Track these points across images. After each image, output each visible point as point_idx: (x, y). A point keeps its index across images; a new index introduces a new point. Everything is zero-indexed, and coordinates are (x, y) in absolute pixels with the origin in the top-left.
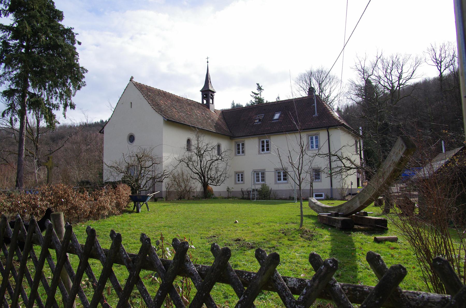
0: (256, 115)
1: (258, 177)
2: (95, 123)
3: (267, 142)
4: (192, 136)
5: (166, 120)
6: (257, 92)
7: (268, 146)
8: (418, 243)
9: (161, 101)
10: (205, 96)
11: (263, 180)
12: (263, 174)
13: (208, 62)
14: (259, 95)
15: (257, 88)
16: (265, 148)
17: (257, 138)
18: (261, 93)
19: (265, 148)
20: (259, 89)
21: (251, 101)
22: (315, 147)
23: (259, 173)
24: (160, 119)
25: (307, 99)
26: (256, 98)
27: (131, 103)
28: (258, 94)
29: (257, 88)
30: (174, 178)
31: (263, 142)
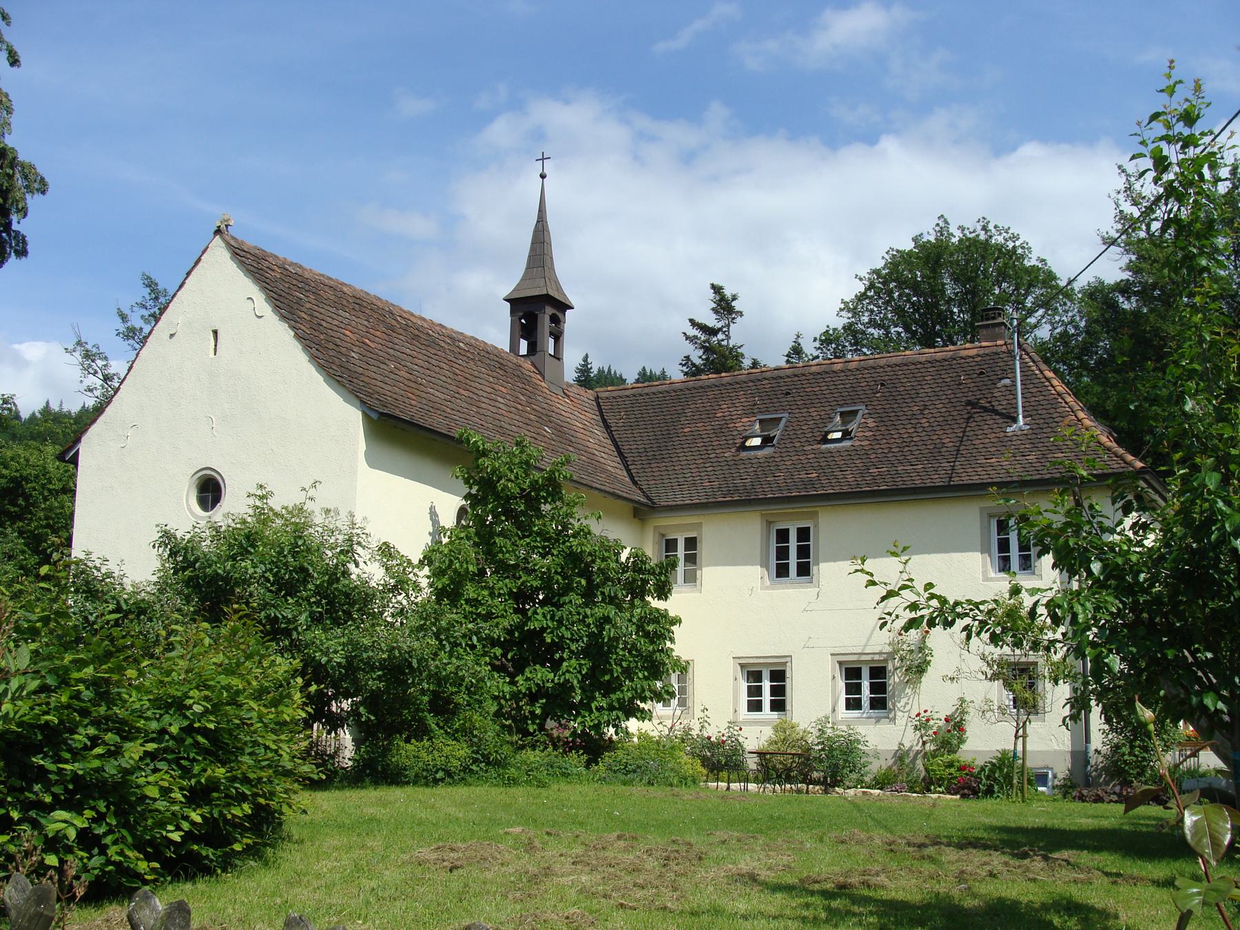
0: (747, 415)
1: (755, 691)
2: (645, 377)
3: (804, 534)
4: (996, 503)
5: (374, 416)
6: (711, 321)
7: (804, 552)
8: (267, 762)
9: (348, 333)
10: (523, 321)
11: (778, 706)
12: (779, 676)
13: (543, 176)
14: (720, 336)
15: (714, 305)
16: (793, 561)
17: (758, 513)
18: (728, 326)
19: (793, 561)
20: (724, 309)
21: (687, 358)
22: (681, 545)
23: (760, 673)
24: (352, 418)
25: (978, 355)
26: (708, 349)
27: (215, 332)
28: (720, 330)
29: (714, 305)
30: (831, 749)
31: (783, 535)
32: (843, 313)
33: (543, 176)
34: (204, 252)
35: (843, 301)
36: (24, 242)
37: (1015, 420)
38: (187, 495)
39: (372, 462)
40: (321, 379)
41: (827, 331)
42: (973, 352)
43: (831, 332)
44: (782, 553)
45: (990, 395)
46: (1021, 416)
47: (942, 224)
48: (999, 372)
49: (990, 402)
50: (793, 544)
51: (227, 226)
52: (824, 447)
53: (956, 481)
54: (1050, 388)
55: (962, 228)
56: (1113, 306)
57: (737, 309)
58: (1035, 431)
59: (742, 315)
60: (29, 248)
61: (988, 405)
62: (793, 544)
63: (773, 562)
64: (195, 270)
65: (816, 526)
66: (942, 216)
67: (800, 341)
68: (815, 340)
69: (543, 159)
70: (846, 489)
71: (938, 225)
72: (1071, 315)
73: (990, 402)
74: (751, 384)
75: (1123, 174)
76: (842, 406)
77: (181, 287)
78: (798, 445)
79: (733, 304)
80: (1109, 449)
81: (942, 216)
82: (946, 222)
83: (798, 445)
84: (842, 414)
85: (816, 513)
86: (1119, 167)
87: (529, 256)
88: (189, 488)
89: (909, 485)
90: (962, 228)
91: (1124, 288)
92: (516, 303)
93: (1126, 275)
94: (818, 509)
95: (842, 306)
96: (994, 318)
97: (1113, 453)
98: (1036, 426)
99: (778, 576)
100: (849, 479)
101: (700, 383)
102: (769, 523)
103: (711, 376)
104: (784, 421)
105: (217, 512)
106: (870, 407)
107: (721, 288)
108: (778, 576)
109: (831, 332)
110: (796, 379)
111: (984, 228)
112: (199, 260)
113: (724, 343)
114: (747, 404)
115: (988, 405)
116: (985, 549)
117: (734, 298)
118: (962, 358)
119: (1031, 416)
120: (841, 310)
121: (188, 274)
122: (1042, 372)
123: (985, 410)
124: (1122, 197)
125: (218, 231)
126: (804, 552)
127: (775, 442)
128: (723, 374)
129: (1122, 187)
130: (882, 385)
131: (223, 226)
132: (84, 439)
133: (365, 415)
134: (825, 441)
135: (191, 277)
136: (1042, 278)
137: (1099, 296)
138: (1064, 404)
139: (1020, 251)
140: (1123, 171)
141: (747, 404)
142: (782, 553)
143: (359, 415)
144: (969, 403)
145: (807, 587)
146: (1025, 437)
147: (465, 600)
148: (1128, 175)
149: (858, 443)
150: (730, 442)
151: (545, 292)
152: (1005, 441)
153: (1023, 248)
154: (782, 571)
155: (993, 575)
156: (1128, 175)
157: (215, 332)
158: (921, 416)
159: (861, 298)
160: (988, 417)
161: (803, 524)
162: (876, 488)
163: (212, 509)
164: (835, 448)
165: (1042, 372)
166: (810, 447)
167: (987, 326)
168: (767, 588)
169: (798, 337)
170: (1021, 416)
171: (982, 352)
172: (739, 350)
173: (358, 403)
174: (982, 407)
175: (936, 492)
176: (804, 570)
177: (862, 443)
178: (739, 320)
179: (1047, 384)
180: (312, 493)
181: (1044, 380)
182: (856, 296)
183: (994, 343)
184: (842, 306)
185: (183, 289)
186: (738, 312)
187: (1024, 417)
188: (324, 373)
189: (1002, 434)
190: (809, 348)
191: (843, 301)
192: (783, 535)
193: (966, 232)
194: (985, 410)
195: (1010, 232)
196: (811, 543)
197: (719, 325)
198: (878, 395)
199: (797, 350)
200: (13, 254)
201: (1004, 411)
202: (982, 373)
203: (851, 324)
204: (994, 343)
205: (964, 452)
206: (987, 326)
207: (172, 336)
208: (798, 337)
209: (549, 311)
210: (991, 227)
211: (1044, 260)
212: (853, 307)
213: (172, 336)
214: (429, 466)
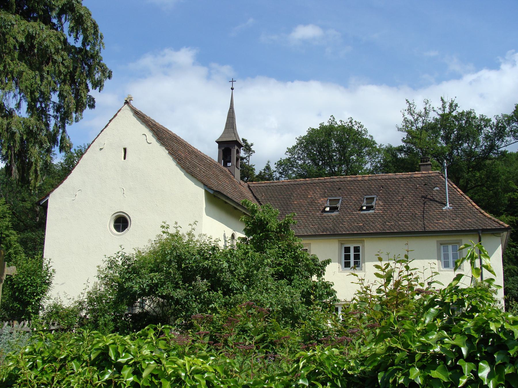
3: (357, 249)
7: (357, 257)
13: (232, 89)
17: (337, 240)
20: (247, 149)
24: (200, 192)
27: (125, 150)
28: (245, 158)
31: (347, 250)
32: (288, 153)
33: (232, 89)
34: (119, 111)
35: (288, 148)
36: (94, 102)
37: (445, 205)
38: (110, 224)
39: (208, 214)
40: (183, 174)
41: (281, 160)
42: (419, 175)
43: (282, 161)
44: (347, 257)
45: (431, 194)
46: (448, 203)
47: (332, 119)
48: (433, 184)
49: (432, 197)
50: (352, 254)
51: (130, 100)
52: (362, 212)
53: (427, 229)
54: (457, 192)
55: (341, 121)
56: (395, 156)
57: (253, 149)
58: (455, 210)
59: (254, 152)
60: (96, 104)
61: (431, 198)
62: (352, 254)
63: (343, 261)
64: (114, 119)
65: (363, 246)
66: (332, 116)
67: (269, 164)
68: (275, 164)
69: (232, 81)
70: (378, 231)
71: (330, 119)
72: (380, 158)
73: (432, 197)
74: (321, 184)
75: (408, 103)
76: (366, 195)
77: (106, 127)
78: (350, 211)
79: (251, 147)
80: (490, 218)
81: (332, 116)
82: (334, 118)
83: (350, 211)
84: (367, 199)
85: (364, 241)
86: (407, 100)
87: (226, 123)
88: (111, 220)
89: (407, 230)
90: (341, 121)
91: (400, 149)
92: (220, 143)
93: (403, 144)
94: (364, 239)
95: (287, 150)
96: (426, 162)
97: (493, 220)
98: (455, 208)
99: (345, 267)
100: (378, 227)
101: (297, 183)
102: (342, 244)
103: (301, 179)
104: (341, 200)
105: (125, 233)
106: (379, 196)
107: (246, 140)
108: (345, 267)
109: (282, 161)
110: (342, 183)
111: (351, 122)
112: (116, 115)
113: (247, 164)
114: (321, 192)
115: (431, 198)
116: (439, 258)
117: (252, 145)
118: (415, 178)
119: (452, 203)
120: (287, 152)
121: (110, 121)
122: (452, 185)
123: (431, 200)
124: (406, 113)
125: (127, 102)
126: (357, 257)
127: (339, 209)
128: (307, 179)
129: (407, 108)
130: (382, 187)
131: (128, 100)
132: (51, 195)
133: (206, 192)
134: (361, 209)
135: (111, 122)
136: (370, 144)
137: (390, 151)
138: (465, 199)
139: (363, 132)
140: (408, 102)
141: (321, 192)
142: (347, 257)
143: (203, 191)
144: (423, 197)
145: (360, 272)
146: (451, 212)
147: (162, 271)
148: (410, 104)
149: (377, 212)
150: (318, 208)
151: (235, 140)
152: (444, 214)
153: (365, 131)
154: (347, 265)
155: (442, 269)
156: (410, 104)
157: (125, 150)
158: (403, 201)
159: (294, 147)
160: (433, 203)
161: (356, 245)
162: (392, 231)
163: (123, 231)
164: (367, 213)
165: (452, 185)
166: (356, 212)
167: (424, 165)
168: (341, 272)
169: (269, 162)
170: (448, 203)
171: (423, 175)
172: (253, 167)
173: (202, 185)
174: (429, 199)
175: (402, 234)
176: (357, 264)
177: (379, 212)
178: (253, 154)
179: (455, 190)
180: (194, 226)
181: (453, 188)
182: (293, 146)
183: (428, 172)
184: (287, 150)
185: (107, 128)
186: (253, 151)
187: (449, 204)
188: (184, 171)
189: (441, 210)
190: (273, 167)
191: (288, 148)
192: (347, 250)
193: (343, 123)
194: (431, 200)
195: (361, 124)
196: (360, 253)
197: (245, 156)
198: (381, 191)
199: (268, 168)
200: (87, 107)
201: (439, 201)
202: (425, 184)
203: (290, 158)
204: (428, 172)
205: (427, 217)
206: (424, 165)
207: (101, 149)
208: (269, 162)
209: (236, 148)
210: (353, 121)
211: (372, 136)
212: (291, 151)
213: (101, 149)
214: (224, 215)
